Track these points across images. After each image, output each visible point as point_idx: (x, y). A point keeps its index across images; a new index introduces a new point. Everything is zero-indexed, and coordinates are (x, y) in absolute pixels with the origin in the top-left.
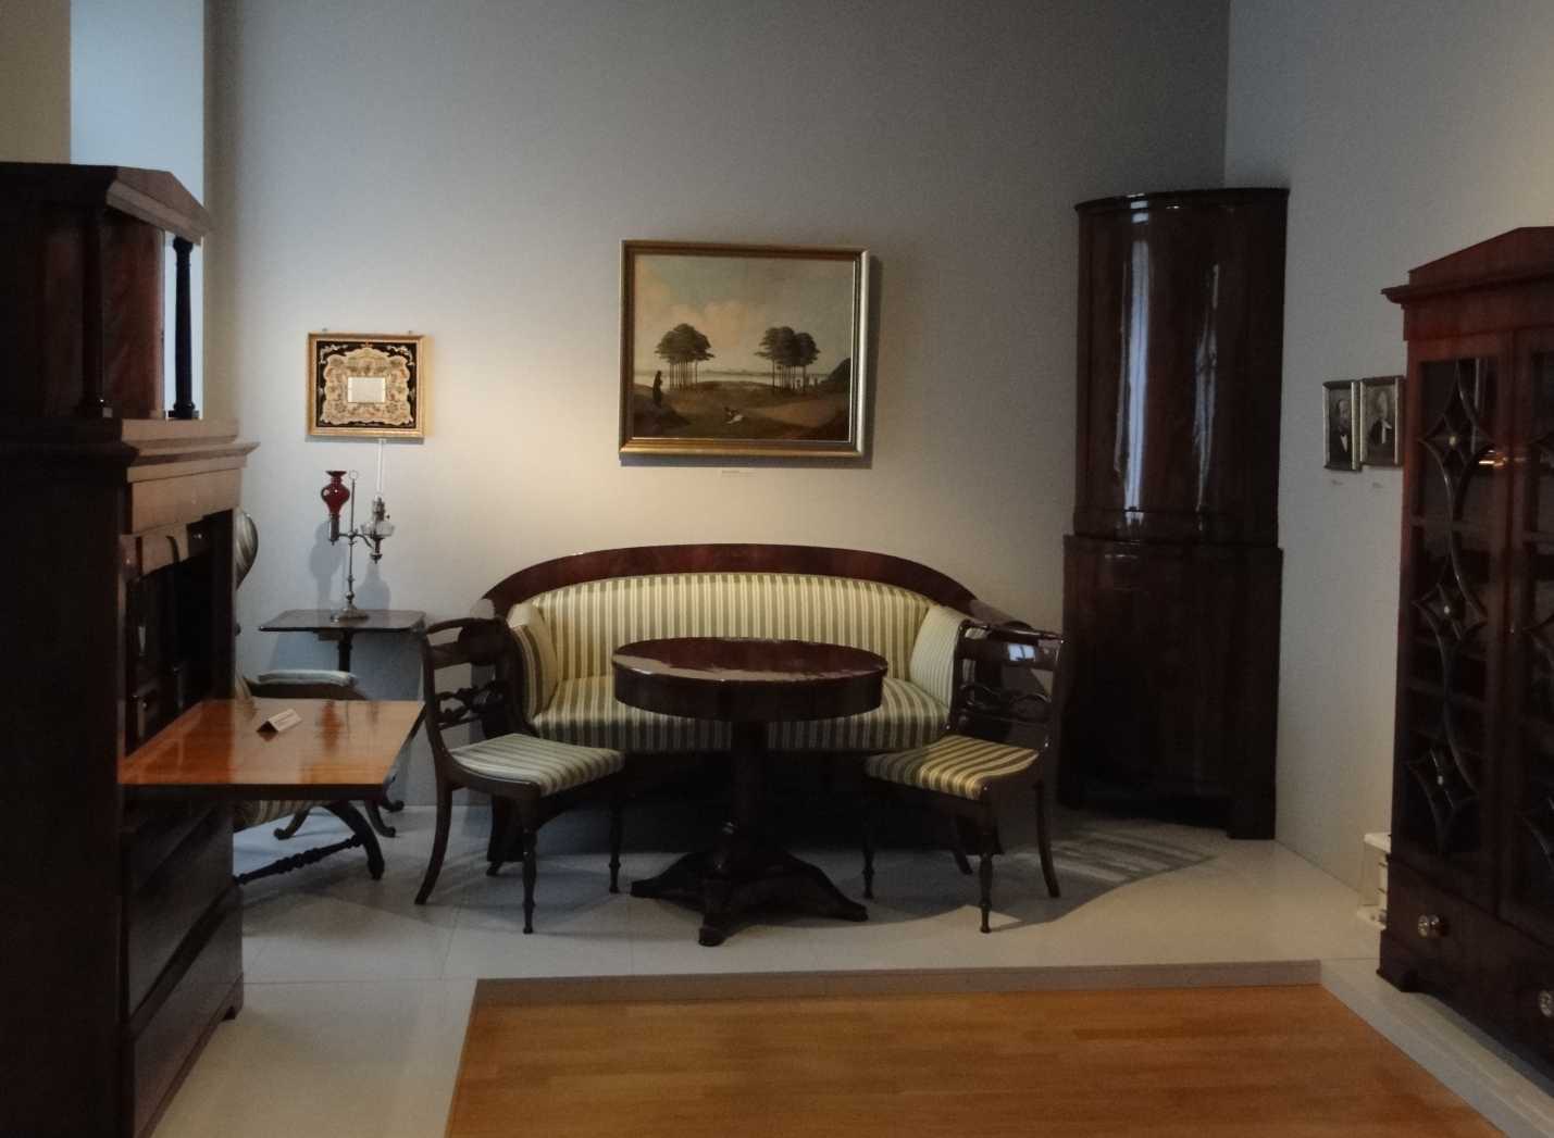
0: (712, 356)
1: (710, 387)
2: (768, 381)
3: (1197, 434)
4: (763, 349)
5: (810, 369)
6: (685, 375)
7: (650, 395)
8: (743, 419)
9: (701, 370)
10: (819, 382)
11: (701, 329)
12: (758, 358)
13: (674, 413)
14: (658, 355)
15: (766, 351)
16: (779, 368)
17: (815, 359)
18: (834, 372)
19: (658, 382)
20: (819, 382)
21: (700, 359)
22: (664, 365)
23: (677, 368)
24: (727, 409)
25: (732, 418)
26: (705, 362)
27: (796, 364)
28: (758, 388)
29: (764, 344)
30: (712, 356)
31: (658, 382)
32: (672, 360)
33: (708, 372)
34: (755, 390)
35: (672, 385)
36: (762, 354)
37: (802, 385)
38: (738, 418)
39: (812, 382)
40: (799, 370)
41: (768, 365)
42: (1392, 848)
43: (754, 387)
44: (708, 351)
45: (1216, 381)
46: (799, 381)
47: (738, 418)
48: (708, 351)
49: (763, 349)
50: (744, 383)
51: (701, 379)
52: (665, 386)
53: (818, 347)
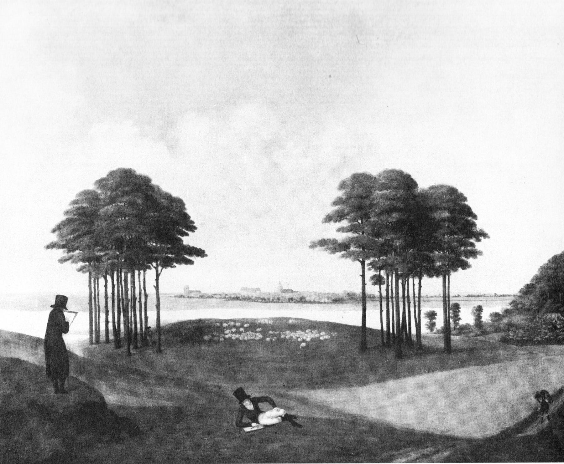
0: (200, 253)
1: (194, 334)
2: (350, 316)
3: (328, 410)
4: (335, 232)
5: (460, 281)
6: (126, 304)
7: (36, 358)
8: (286, 418)
9: (174, 294)
10: (486, 317)
11: (167, 181)
12: (324, 256)
13: (103, 404)
14: (60, 253)
15: (341, 237)
16: (378, 280)
17: (474, 254)
18: (528, 290)
19: (58, 324)
20: (486, 317)
21: (167, 263)
22: (74, 281)
23: (105, 286)
24: (241, 395)
25: (254, 416)
26: (181, 268)
27: (423, 267)
28: (324, 336)
29: (338, 216)
30: (200, 253)
31: (58, 324)
32: (94, 265)
33: (192, 296)
34: (314, 344)
35: (95, 332)
36: (334, 246)
37: (440, 323)
38: (270, 417)
39: (467, 317)
40: (431, 285)
41: (348, 273)
42: (64, 317)
43: (309, 336)
44: (188, 240)
45: (162, 408)
46: (432, 315)
47: (270, 417)
48: (188, 240)
49: (335, 232)
50: (283, 325)
51: (172, 316)
52: (76, 339)
53: (480, 224)
